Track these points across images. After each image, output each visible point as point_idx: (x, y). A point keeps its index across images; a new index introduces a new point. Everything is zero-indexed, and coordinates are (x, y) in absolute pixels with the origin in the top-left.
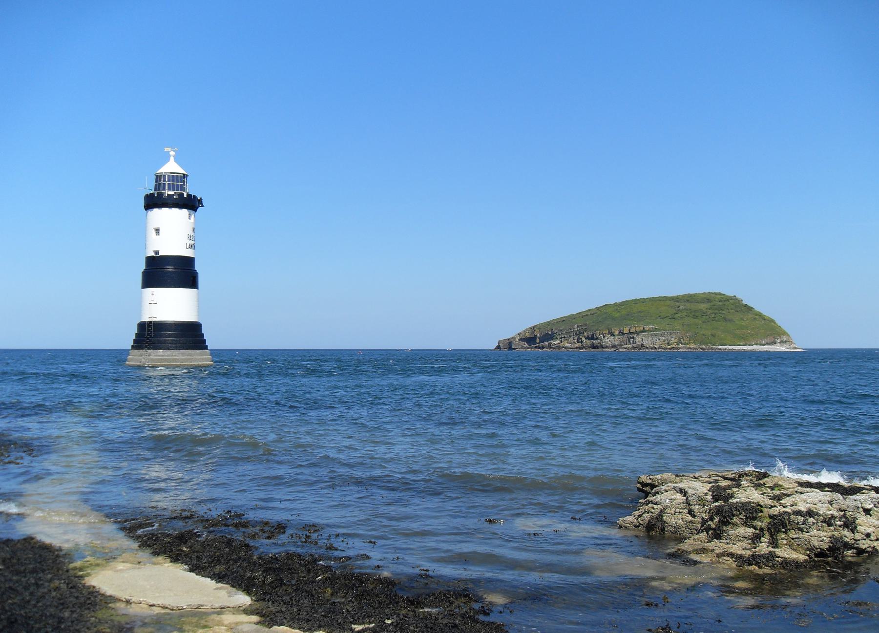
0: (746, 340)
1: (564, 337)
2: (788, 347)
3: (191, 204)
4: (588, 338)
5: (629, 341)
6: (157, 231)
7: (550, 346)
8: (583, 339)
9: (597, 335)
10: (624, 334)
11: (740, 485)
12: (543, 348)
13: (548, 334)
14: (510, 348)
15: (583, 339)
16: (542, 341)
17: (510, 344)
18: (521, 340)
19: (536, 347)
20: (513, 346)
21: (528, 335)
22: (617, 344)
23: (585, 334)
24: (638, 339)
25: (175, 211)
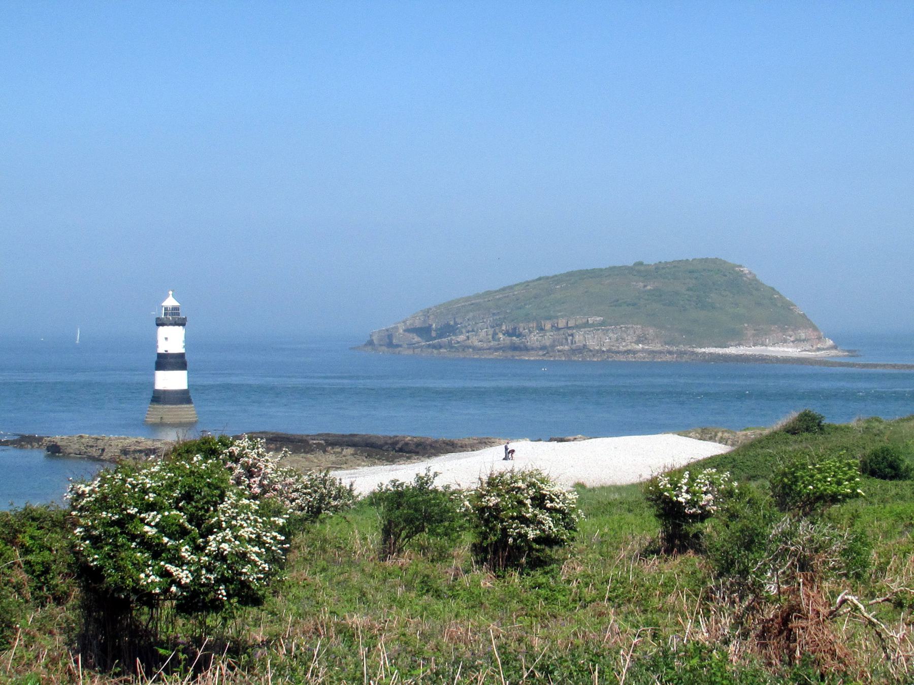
0: (737, 337)
1: (473, 331)
3: (182, 323)
4: (508, 334)
5: (567, 339)
6: (166, 351)
7: (450, 346)
8: (501, 336)
10: (558, 329)
12: (440, 347)
13: (448, 325)
14: (390, 345)
16: (440, 336)
17: (390, 337)
18: (407, 330)
20: (394, 341)
21: (418, 324)
22: (548, 344)
23: (504, 328)
25: (177, 327)
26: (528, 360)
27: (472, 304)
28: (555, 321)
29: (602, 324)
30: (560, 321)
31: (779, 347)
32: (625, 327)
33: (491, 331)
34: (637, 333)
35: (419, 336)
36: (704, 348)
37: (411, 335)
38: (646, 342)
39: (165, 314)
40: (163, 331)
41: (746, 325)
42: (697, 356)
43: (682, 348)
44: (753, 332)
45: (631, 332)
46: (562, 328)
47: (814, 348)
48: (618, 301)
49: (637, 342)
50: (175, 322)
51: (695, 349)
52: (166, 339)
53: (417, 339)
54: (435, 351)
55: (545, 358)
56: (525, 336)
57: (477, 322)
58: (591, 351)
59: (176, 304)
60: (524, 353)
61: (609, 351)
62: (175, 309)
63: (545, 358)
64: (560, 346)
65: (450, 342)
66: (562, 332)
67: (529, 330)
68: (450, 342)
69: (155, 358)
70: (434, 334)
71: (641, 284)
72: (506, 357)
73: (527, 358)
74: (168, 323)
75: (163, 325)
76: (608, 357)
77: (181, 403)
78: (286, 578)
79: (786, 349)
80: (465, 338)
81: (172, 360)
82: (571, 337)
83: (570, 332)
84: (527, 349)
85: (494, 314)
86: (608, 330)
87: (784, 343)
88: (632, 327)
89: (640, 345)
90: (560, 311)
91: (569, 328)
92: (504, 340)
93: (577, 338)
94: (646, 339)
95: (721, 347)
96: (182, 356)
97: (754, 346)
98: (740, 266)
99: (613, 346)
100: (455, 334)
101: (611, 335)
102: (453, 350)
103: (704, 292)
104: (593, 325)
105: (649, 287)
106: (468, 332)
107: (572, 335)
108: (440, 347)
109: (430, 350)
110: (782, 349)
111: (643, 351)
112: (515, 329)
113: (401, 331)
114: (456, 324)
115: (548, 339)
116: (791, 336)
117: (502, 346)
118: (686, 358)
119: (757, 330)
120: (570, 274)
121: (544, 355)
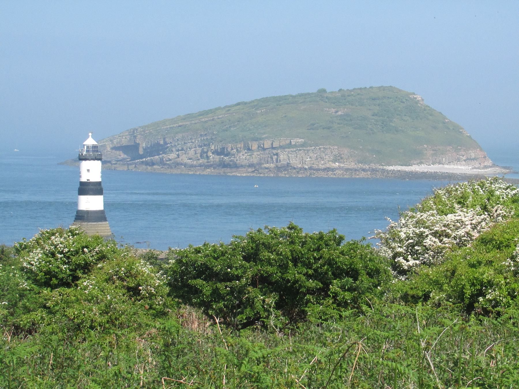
1: (182, 150)
2: (477, 165)
4: (216, 152)
5: (272, 158)
6: (88, 180)
7: (162, 162)
8: (210, 154)
9: (229, 149)
10: (264, 149)
11: (402, 240)
12: (153, 164)
13: (158, 144)
15: (210, 154)
19: (143, 162)
21: (125, 142)
22: (255, 162)
24: (283, 157)
25: (96, 161)
26: (241, 176)
27: (180, 126)
28: (262, 142)
29: (303, 145)
30: (265, 142)
31: (454, 164)
32: (324, 148)
33: (199, 150)
34: (334, 153)
35: (125, 154)
36: (392, 165)
37: (118, 152)
38: (342, 161)
39: (87, 151)
40: (85, 165)
41: (425, 146)
42: (388, 173)
43: (373, 166)
44: (432, 152)
45: (329, 151)
46: (268, 149)
47: (482, 166)
48: (314, 125)
49: (334, 161)
50: (95, 157)
51: (385, 167)
52: (88, 170)
53: (123, 156)
54: (149, 168)
55: (255, 174)
56: (234, 155)
57: (186, 142)
58: (295, 168)
59: (95, 143)
60: (234, 170)
61: (311, 168)
62: (94, 147)
63: (255, 174)
64: (266, 164)
65: (162, 159)
66: (267, 151)
67: (237, 150)
68: (162, 159)
69: (78, 185)
70: (141, 152)
71: (333, 110)
72: (219, 173)
73: (239, 175)
74: (90, 158)
75: (86, 159)
76: (311, 174)
77: (101, 221)
78: (451, 323)
79: (460, 167)
80: (176, 156)
81: (92, 187)
82: (276, 157)
83: (275, 152)
84: (236, 166)
85: (201, 135)
86: (308, 151)
87: (458, 162)
88: (330, 148)
89: (337, 163)
90: (264, 133)
91: (273, 148)
92: (213, 158)
93: (282, 157)
94: (342, 158)
95: (406, 166)
96: (99, 183)
97: (433, 164)
98: (414, 94)
99: (313, 164)
100: (164, 153)
101: (311, 155)
102: (166, 167)
103: (388, 117)
104: (295, 146)
105: (340, 113)
106: (178, 150)
107: (277, 154)
108: (153, 164)
109: (144, 167)
110: (456, 167)
111: (340, 168)
112: (224, 148)
113: (109, 149)
114: (166, 143)
115: (255, 159)
116: (463, 156)
117: (212, 163)
118: (379, 176)
119: (435, 150)
120: (266, 101)
121: (253, 172)
